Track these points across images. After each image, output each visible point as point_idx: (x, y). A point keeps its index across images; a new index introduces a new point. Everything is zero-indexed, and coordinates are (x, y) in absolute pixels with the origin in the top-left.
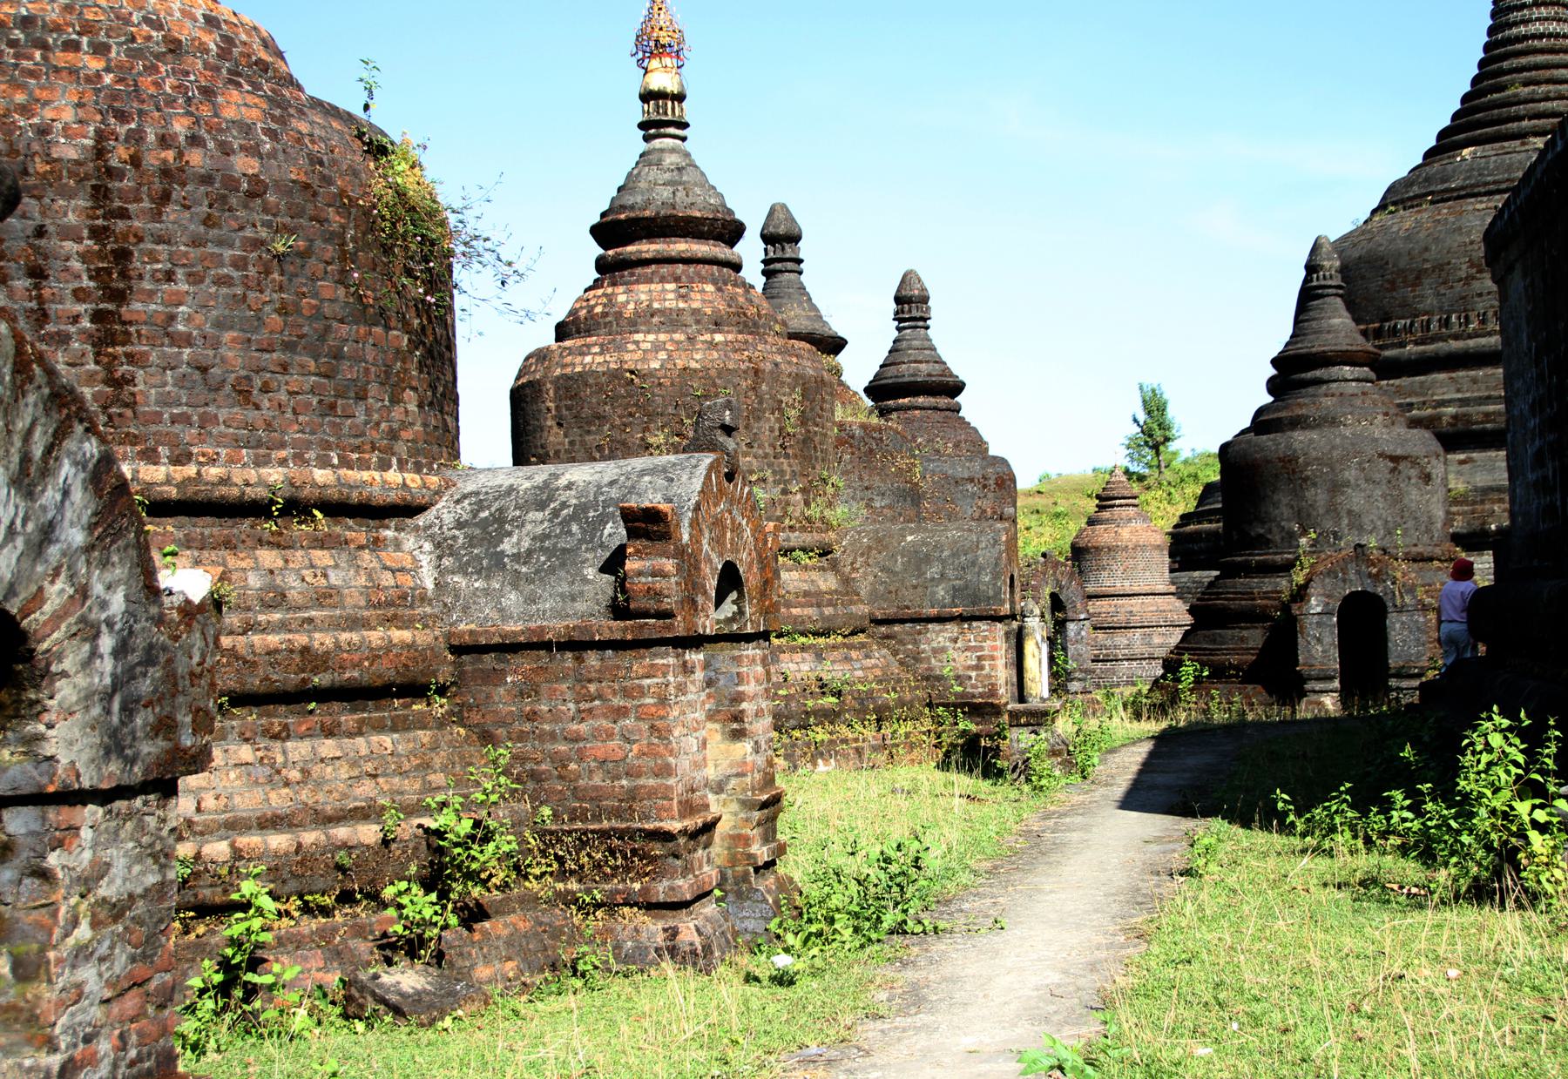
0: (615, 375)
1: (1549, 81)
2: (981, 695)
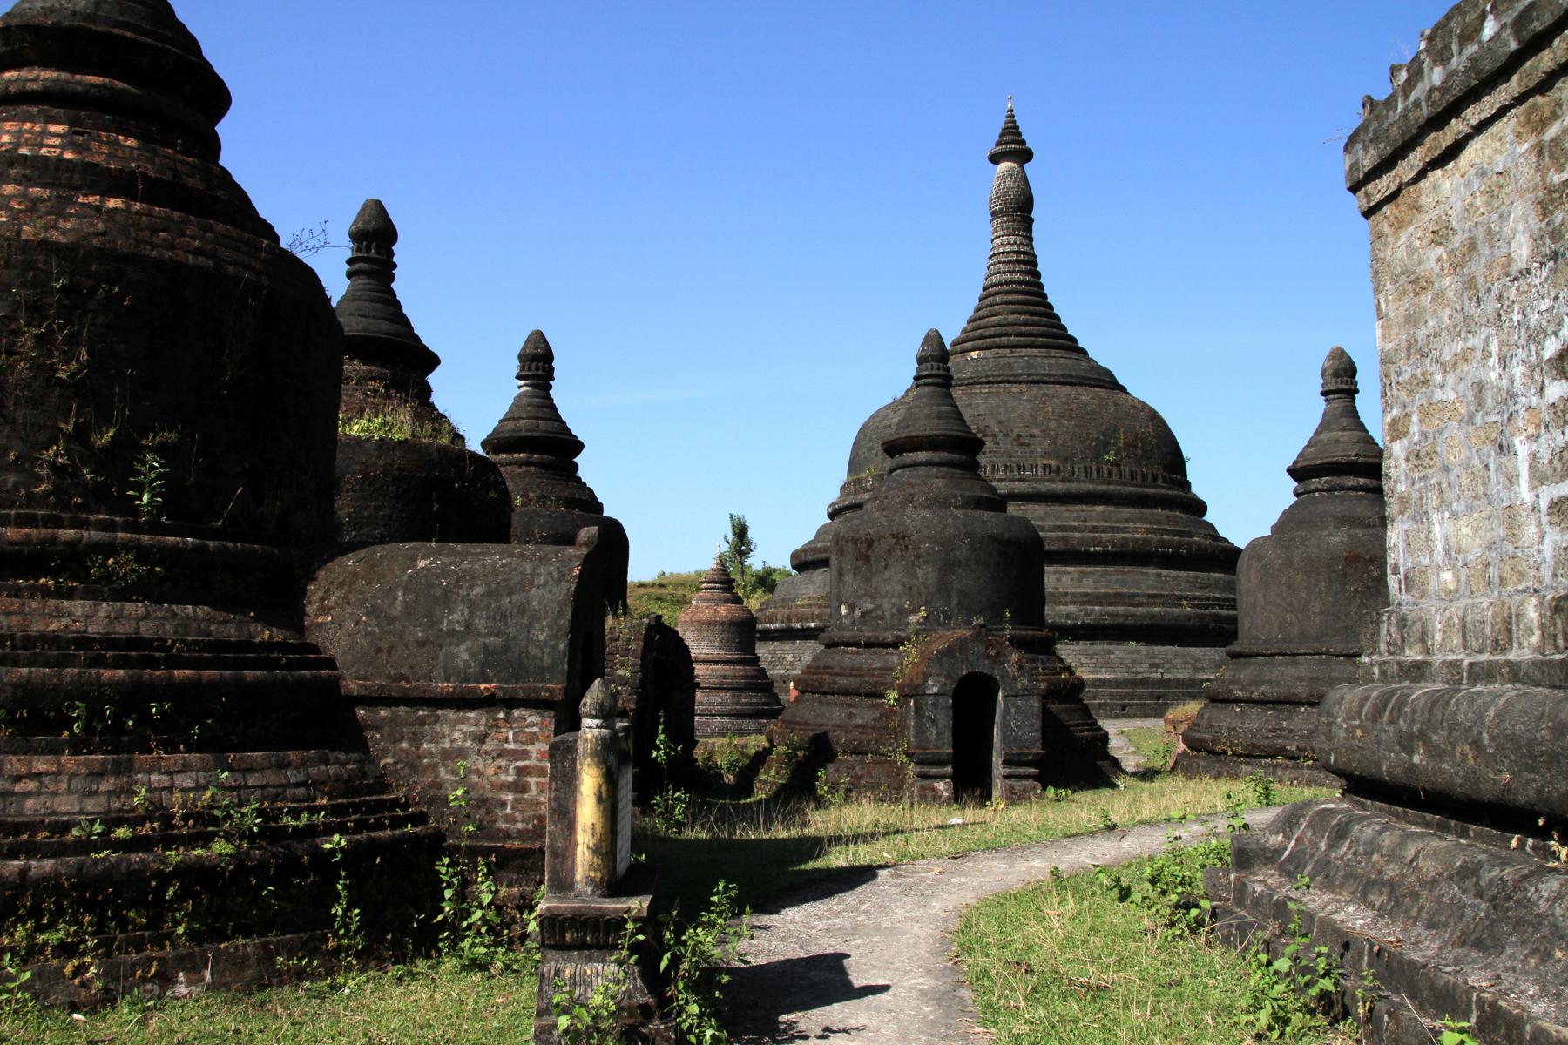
2: (521, 835)
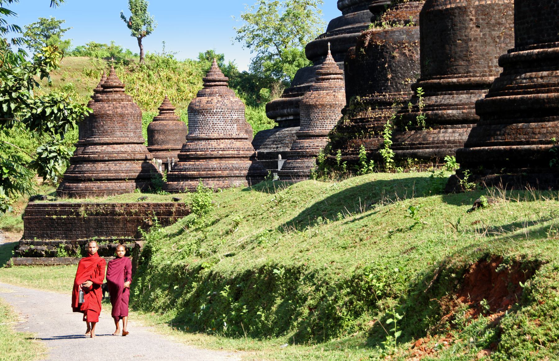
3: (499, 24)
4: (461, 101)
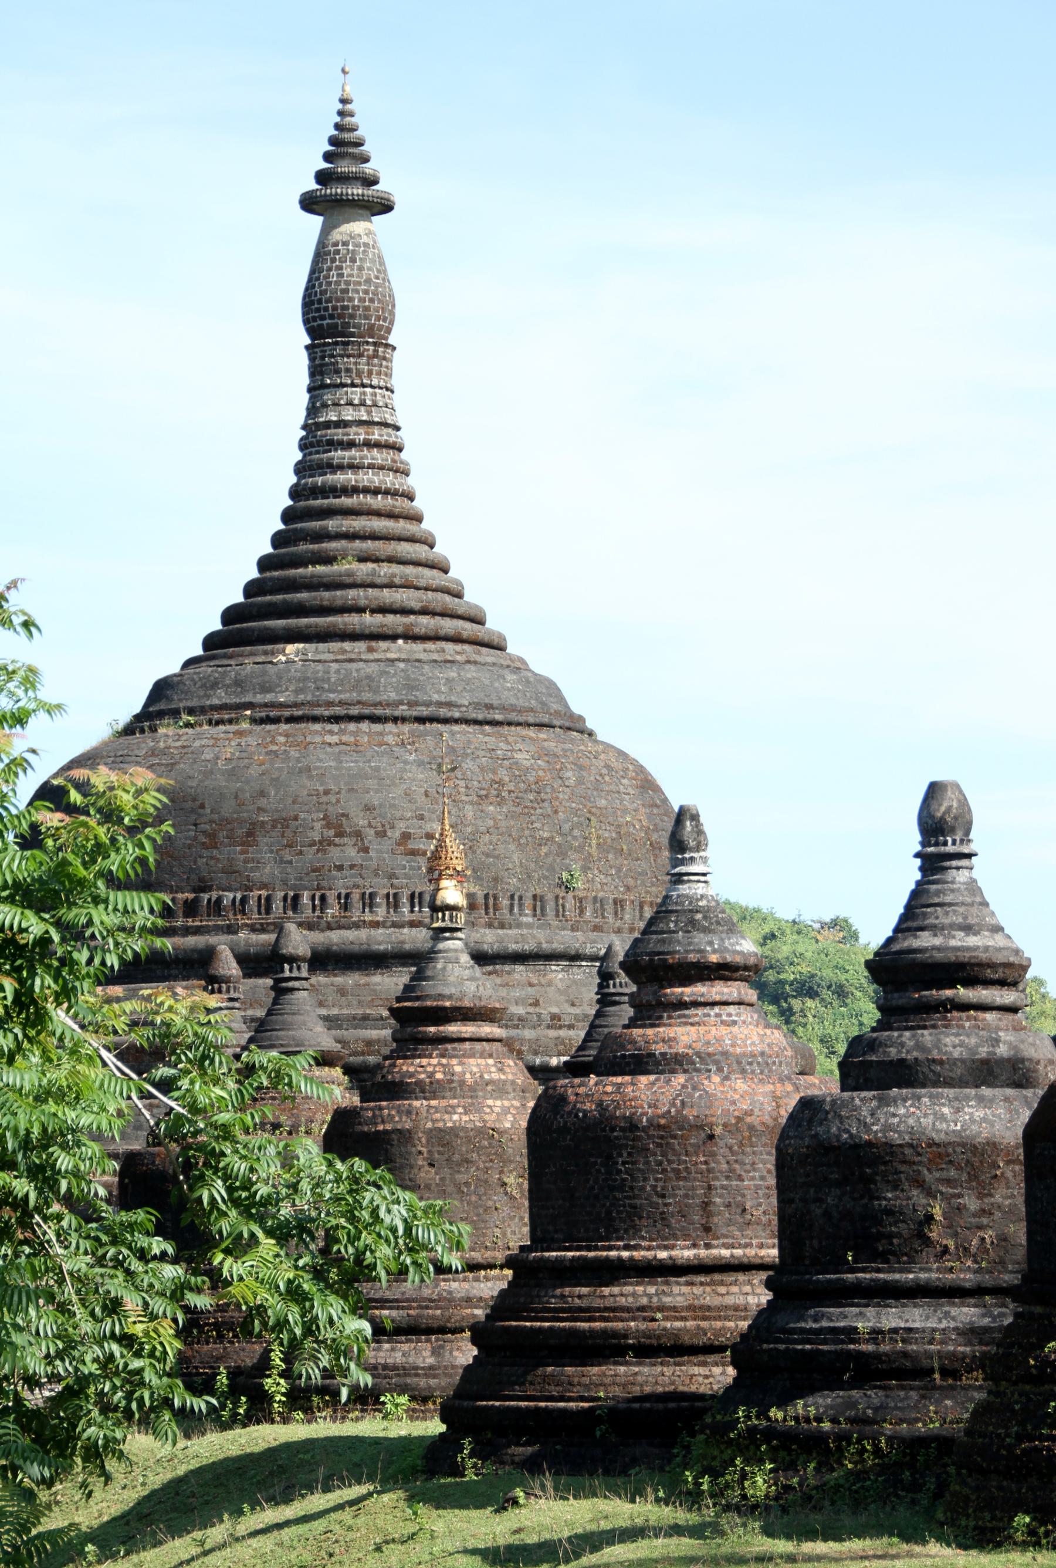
0: (480, 1132)
1: (390, 560)
3: (467, 1161)
4: (403, 1293)
